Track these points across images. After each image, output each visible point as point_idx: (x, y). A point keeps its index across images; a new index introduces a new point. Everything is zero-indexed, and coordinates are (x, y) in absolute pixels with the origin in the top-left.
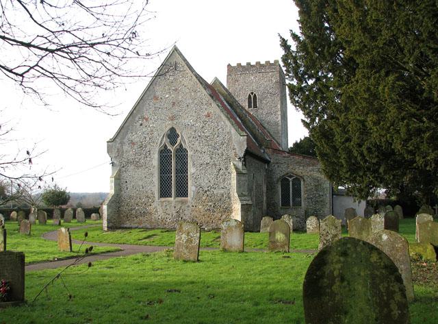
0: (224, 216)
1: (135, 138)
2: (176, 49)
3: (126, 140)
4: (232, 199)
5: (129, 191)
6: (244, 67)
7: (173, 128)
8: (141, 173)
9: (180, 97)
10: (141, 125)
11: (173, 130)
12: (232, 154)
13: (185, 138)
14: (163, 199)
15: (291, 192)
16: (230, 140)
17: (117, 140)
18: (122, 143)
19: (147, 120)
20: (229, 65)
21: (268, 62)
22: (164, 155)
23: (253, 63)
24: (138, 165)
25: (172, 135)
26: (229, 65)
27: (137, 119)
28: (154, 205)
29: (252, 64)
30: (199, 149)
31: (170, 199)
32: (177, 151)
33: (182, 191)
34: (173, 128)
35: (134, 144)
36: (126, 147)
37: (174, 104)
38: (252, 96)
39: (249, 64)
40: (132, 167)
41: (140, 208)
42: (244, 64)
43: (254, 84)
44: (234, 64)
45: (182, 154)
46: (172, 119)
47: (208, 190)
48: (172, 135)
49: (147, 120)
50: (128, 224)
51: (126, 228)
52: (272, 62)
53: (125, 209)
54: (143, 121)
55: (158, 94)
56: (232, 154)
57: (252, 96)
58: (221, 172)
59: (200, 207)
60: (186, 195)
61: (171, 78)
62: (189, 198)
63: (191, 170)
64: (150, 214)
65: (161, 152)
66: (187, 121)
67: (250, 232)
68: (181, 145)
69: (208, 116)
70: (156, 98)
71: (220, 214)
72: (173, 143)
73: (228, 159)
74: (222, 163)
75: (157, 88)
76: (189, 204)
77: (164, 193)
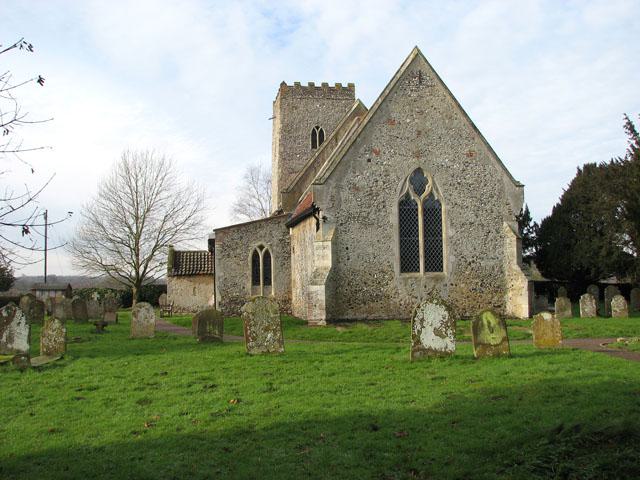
0: (496, 298)
1: (359, 180)
2: (417, 56)
3: (344, 183)
4: (507, 273)
5: (354, 262)
6: (304, 88)
7: (419, 168)
8: (370, 235)
9: (428, 124)
10: (369, 160)
11: (419, 171)
12: (505, 212)
13: (436, 185)
14: (407, 275)
15: (261, 268)
16: (501, 191)
17: (330, 181)
18: (339, 188)
19: (377, 153)
20: (283, 84)
21: (339, 85)
22: (406, 209)
23: (318, 84)
24: (366, 223)
25: (418, 180)
26: (283, 84)
27: (362, 150)
28: (392, 285)
29: (330, 86)
30: (459, 202)
31: (417, 274)
32: (425, 202)
33: (434, 263)
34: (419, 168)
35: (357, 189)
36: (345, 194)
37: (419, 133)
38: (317, 132)
39: (311, 85)
40: (357, 225)
41: (370, 289)
42: (305, 84)
43: (320, 115)
44: (290, 83)
45: (433, 213)
46: (418, 155)
47: (473, 262)
48: (418, 180)
49: (377, 153)
50: (350, 315)
51: (348, 321)
52: (345, 85)
53: (345, 290)
54: (371, 154)
55: (393, 115)
56: (505, 212)
57: (317, 132)
58: (491, 236)
59: (463, 285)
60: (440, 269)
61: (414, 95)
62: (445, 272)
63: (447, 232)
64: (388, 297)
65: (402, 204)
66: (440, 160)
67: (29, 336)
68: (431, 194)
69: (470, 155)
70: (392, 122)
71: (490, 296)
72: (419, 192)
73: (500, 219)
74: (492, 224)
75: (392, 106)
76: (446, 281)
77: (408, 264)
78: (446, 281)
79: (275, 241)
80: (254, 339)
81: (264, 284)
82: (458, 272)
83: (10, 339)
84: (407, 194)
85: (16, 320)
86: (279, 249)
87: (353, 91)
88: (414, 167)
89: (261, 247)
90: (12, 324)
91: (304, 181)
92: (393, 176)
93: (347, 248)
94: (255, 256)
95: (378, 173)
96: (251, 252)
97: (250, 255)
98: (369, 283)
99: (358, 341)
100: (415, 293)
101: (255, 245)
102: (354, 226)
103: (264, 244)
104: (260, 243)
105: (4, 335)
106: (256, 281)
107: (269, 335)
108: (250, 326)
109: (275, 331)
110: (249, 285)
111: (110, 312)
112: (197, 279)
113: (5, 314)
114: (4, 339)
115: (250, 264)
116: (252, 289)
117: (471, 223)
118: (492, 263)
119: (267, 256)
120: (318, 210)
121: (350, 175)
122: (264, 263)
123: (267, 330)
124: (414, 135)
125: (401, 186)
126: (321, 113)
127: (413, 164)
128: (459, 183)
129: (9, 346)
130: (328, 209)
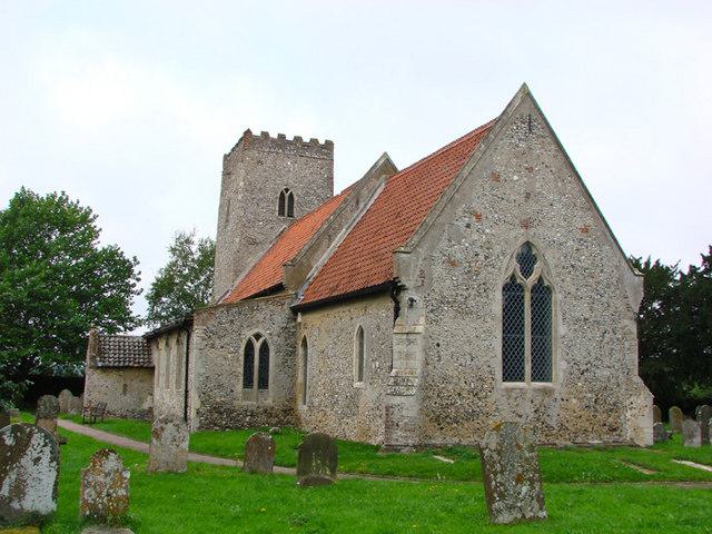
1: (457, 252)
2: (525, 95)
8: (469, 326)
11: (528, 245)
19: (479, 217)
20: (248, 132)
22: (512, 289)
24: (463, 311)
25: (527, 259)
26: (248, 132)
30: (573, 290)
37: (528, 196)
39: (282, 137)
41: (465, 403)
44: (256, 132)
46: (526, 225)
48: (527, 259)
49: (479, 217)
57: (287, 195)
65: (506, 288)
67: (56, 484)
72: (527, 272)
77: (512, 371)
78: (556, 395)
79: (276, 329)
80: (502, 496)
81: (260, 387)
82: (570, 383)
83: (19, 490)
84: (513, 277)
85: (31, 453)
86: (281, 341)
87: (332, 151)
88: (522, 240)
89: (258, 336)
90: (23, 461)
91: (316, 250)
92: (497, 249)
93: (438, 345)
94: (249, 346)
95: (479, 244)
96: (245, 342)
97: (243, 348)
98: (464, 394)
99: (232, 458)
100: (521, 412)
101: (249, 334)
102: (448, 314)
103: (262, 332)
104: (256, 331)
105: (7, 481)
106: (248, 382)
107: (524, 489)
108: (495, 473)
109: (532, 481)
110: (240, 386)
111: (46, 418)
112: (129, 374)
113: (9, 441)
114: (5, 491)
115: (242, 358)
116: (244, 394)
117: (586, 319)
118: (607, 373)
119: (265, 348)
120: (402, 288)
121: (443, 244)
122: (261, 362)
123: (519, 480)
124: (522, 200)
125: (508, 266)
126: (292, 173)
127: (518, 237)
128: (573, 266)
129: (15, 505)
130: (417, 288)
